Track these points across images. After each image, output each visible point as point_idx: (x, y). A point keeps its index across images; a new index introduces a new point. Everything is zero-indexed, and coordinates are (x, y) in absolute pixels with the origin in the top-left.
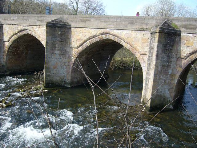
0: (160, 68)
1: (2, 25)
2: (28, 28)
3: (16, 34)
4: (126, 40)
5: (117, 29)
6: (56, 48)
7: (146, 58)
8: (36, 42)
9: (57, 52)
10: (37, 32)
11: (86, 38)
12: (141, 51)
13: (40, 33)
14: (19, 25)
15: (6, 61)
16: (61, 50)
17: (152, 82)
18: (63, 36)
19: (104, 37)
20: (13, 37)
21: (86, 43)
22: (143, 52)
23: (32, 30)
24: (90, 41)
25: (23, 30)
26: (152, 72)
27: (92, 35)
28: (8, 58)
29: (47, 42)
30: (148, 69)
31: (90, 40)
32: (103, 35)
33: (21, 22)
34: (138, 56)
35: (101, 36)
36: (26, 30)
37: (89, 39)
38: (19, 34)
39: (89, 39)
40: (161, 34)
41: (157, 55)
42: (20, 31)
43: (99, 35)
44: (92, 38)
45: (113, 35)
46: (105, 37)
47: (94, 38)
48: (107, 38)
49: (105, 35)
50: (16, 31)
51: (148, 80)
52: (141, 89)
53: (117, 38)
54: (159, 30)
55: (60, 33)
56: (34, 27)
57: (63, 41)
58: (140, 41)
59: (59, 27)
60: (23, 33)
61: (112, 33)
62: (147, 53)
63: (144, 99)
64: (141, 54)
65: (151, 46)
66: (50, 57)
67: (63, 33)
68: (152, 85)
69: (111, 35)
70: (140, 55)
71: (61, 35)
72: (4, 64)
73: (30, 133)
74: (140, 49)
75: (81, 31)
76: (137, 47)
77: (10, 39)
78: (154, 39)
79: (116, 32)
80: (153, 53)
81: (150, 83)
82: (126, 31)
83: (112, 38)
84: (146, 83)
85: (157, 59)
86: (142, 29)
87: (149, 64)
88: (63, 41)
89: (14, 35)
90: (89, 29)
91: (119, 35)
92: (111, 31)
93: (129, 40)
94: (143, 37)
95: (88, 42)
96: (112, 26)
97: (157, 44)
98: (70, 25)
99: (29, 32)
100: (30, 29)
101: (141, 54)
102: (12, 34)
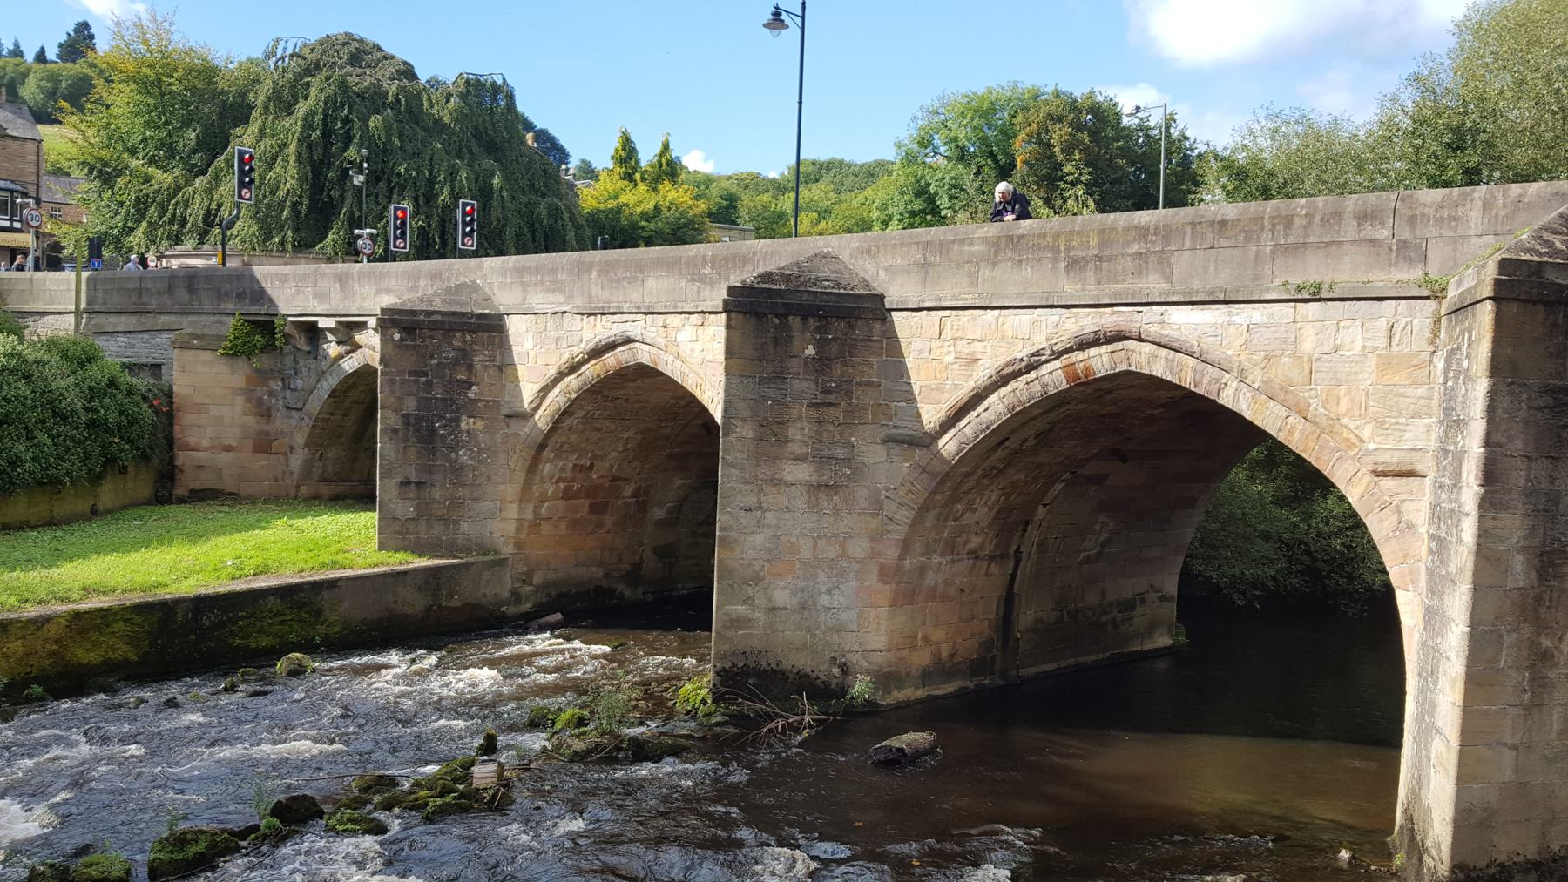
0: (1519, 570)
1: (500, 317)
2: (634, 327)
3: (573, 368)
4: (1256, 376)
5: (1192, 303)
6: (796, 448)
7: (1418, 503)
8: (690, 405)
9: (802, 472)
10: (685, 349)
11: (983, 373)
12: (1372, 446)
13: (695, 355)
14: (590, 314)
15: (518, 529)
16: (820, 460)
17: (1460, 685)
18: (837, 369)
19: (1101, 361)
20: (556, 390)
21: (980, 409)
22: (1390, 460)
23: (661, 341)
24: (1003, 391)
25: (612, 346)
26: (1458, 605)
27: (1022, 353)
28: (529, 515)
29: (725, 411)
30: (1437, 584)
31: (1005, 384)
32: (1093, 351)
33: (601, 293)
34: (1355, 489)
35: (1078, 356)
36: (629, 341)
37: (561, 376)
38: (591, 370)
39: (1002, 380)
40: (1514, 307)
41: (1489, 476)
42: (597, 352)
43: (1069, 350)
44: (1019, 373)
45: (1159, 344)
46: (1105, 358)
47: (1033, 375)
48: (1124, 367)
49: (1104, 348)
50: (576, 350)
51: (1430, 673)
52: (1393, 740)
53: (1191, 362)
54: (1497, 282)
55: (810, 351)
56: (671, 319)
57: (831, 399)
58: (1368, 376)
59: (806, 312)
60: (611, 360)
61: (1152, 331)
62: (1426, 464)
63: (1410, 820)
64: (1377, 474)
65: (1447, 410)
66: (751, 500)
67: (834, 349)
68: (1460, 703)
69: (1147, 348)
70: (1368, 478)
71: (822, 364)
72: (508, 550)
73: (1209, 878)
74: (1366, 433)
75: (947, 333)
76: (1345, 421)
77: (543, 398)
78: (1469, 356)
79: (1184, 322)
80: (1459, 457)
81: (1448, 689)
82: (1256, 313)
83: (1156, 364)
84: (1422, 691)
85: (1489, 503)
86: (1299, 289)
87: (1440, 547)
88: (831, 399)
89: (561, 376)
90: (996, 312)
91: (1208, 343)
92: (1145, 320)
93: (1285, 368)
94: (1383, 342)
95: (993, 398)
96: (1153, 285)
97: (1481, 387)
98: (880, 298)
99: (644, 355)
100: (650, 335)
101: (1377, 474)
102: (552, 372)
